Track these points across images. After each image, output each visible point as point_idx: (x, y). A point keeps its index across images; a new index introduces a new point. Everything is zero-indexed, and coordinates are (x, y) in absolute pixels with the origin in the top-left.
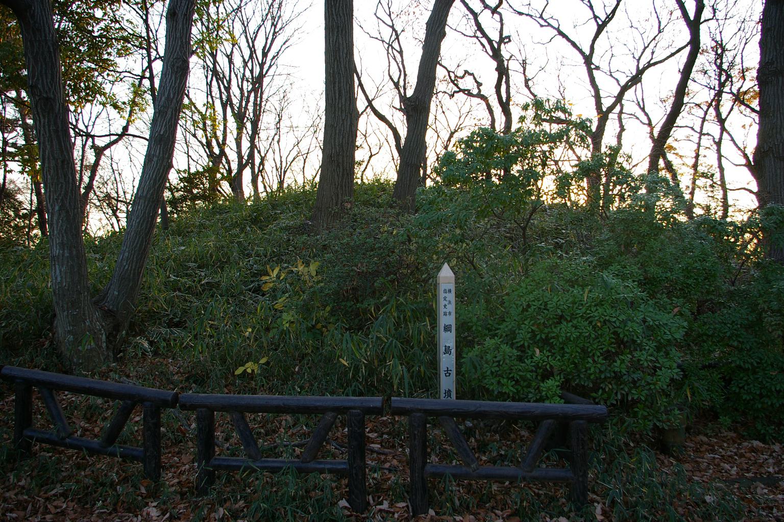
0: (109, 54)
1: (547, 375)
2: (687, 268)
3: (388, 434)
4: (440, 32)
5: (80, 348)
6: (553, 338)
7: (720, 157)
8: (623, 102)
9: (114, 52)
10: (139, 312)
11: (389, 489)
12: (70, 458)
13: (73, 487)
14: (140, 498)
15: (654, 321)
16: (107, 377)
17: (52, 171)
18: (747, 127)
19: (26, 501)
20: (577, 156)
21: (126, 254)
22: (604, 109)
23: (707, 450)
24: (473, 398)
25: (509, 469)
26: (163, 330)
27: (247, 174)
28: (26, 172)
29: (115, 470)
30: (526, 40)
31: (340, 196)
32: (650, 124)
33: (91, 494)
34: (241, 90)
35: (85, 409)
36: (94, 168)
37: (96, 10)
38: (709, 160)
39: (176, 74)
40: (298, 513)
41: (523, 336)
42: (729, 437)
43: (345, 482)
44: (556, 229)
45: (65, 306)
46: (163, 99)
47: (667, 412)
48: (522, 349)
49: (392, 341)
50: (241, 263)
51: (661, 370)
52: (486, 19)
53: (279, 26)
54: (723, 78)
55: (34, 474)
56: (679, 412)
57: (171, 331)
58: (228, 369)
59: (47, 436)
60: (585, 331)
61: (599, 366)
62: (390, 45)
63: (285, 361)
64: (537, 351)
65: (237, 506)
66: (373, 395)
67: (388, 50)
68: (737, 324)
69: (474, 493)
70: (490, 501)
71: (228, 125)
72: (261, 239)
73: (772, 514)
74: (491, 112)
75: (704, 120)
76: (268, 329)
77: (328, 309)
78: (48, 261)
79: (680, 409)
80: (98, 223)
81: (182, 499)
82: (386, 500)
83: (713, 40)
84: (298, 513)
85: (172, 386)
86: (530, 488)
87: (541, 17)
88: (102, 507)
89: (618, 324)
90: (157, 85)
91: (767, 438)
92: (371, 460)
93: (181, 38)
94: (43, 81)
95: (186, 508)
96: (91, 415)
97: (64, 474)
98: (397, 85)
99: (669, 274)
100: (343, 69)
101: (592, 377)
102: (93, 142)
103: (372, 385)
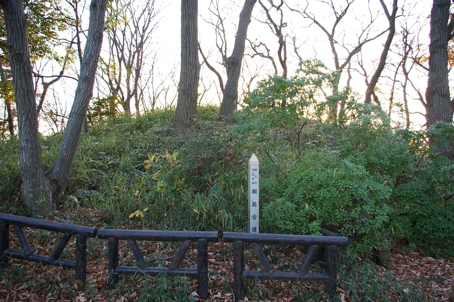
0: (53, 29)
1: (312, 219)
2: (392, 158)
3: (219, 253)
4: (247, 20)
5: (37, 202)
6: (316, 197)
7: (405, 94)
8: (350, 62)
9: (57, 27)
10: (72, 180)
11: (221, 285)
12: (31, 267)
13: (34, 285)
14: (74, 291)
15: (373, 188)
16: (53, 219)
17: (21, 97)
18: (420, 77)
19: (6, 293)
20: (324, 93)
21: (65, 146)
22: (340, 66)
23: (402, 263)
24: (269, 232)
25: (292, 274)
26: (86, 191)
27: (133, 101)
28: (4, 97)
29: (59, 274)
30: (296, 27)
31: (189, 114)
32: (365, 75)
33: (45, 288)
34: (130, 51)
35: (40, 238)
36: (43, 96)
37: (46, 2)
38: (399, 97)
39: (95, 41)
40: (168, 300)
41: (298, 196)
42: (414, 255)
43: (195, 281)
44: (314, 134)
45: (28, 177)
46: (88, 55)
47: (381, 241)
48: (297, 203)
49: (222, 199)
50: (131, 152)
51: (378, 216)
52: (273, 13)
53: (153, 14)
54: (407, 49)
55: (11, 276)
56: (387, 241)
57: (90, 192)
58: (125, 214)
59: (18, 254)
60: (334, 193)
61: (342, 214)
62: (217, 27)
63: (159, 210)
64: (307, 205)
65: (132, 295)
66: (210, 230)
67: (216, 30)
68: (420, 190)
69: (271, 287)
70: (280, 292)
71: (122, 71)
72: (143, 138)
73: (441, 299)
74: (275, 67)
75: (396, 73)
76: (147, 191)
77: (183, 179)
78: (16, 150)
79: (387, 239)
80: (45, 128)
81: (99, 291)
82: (219, 291)
83: (402, 27)
84: (168, 300)
85: (92, 225)
86: (303, 285)
87: (304, 12)
88: (52, 296)
89: (354, 190)
90: (83, 47)
91: (436, 255)
92: (210, 268)
93: (99, 20)
94: (16, 43)
95: (101, 297)
96: (43, 241)
97: (28, 277)
98: (221, 50)
99: (381, 161)
100: (192, 40)
101: (339, 220)
102: (43, 80)
103: (210, 224)
